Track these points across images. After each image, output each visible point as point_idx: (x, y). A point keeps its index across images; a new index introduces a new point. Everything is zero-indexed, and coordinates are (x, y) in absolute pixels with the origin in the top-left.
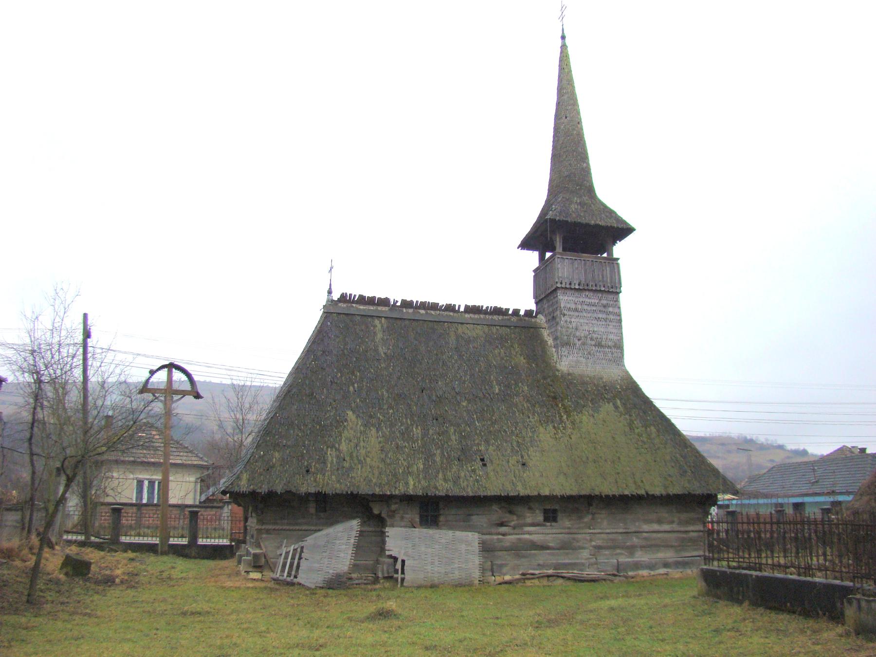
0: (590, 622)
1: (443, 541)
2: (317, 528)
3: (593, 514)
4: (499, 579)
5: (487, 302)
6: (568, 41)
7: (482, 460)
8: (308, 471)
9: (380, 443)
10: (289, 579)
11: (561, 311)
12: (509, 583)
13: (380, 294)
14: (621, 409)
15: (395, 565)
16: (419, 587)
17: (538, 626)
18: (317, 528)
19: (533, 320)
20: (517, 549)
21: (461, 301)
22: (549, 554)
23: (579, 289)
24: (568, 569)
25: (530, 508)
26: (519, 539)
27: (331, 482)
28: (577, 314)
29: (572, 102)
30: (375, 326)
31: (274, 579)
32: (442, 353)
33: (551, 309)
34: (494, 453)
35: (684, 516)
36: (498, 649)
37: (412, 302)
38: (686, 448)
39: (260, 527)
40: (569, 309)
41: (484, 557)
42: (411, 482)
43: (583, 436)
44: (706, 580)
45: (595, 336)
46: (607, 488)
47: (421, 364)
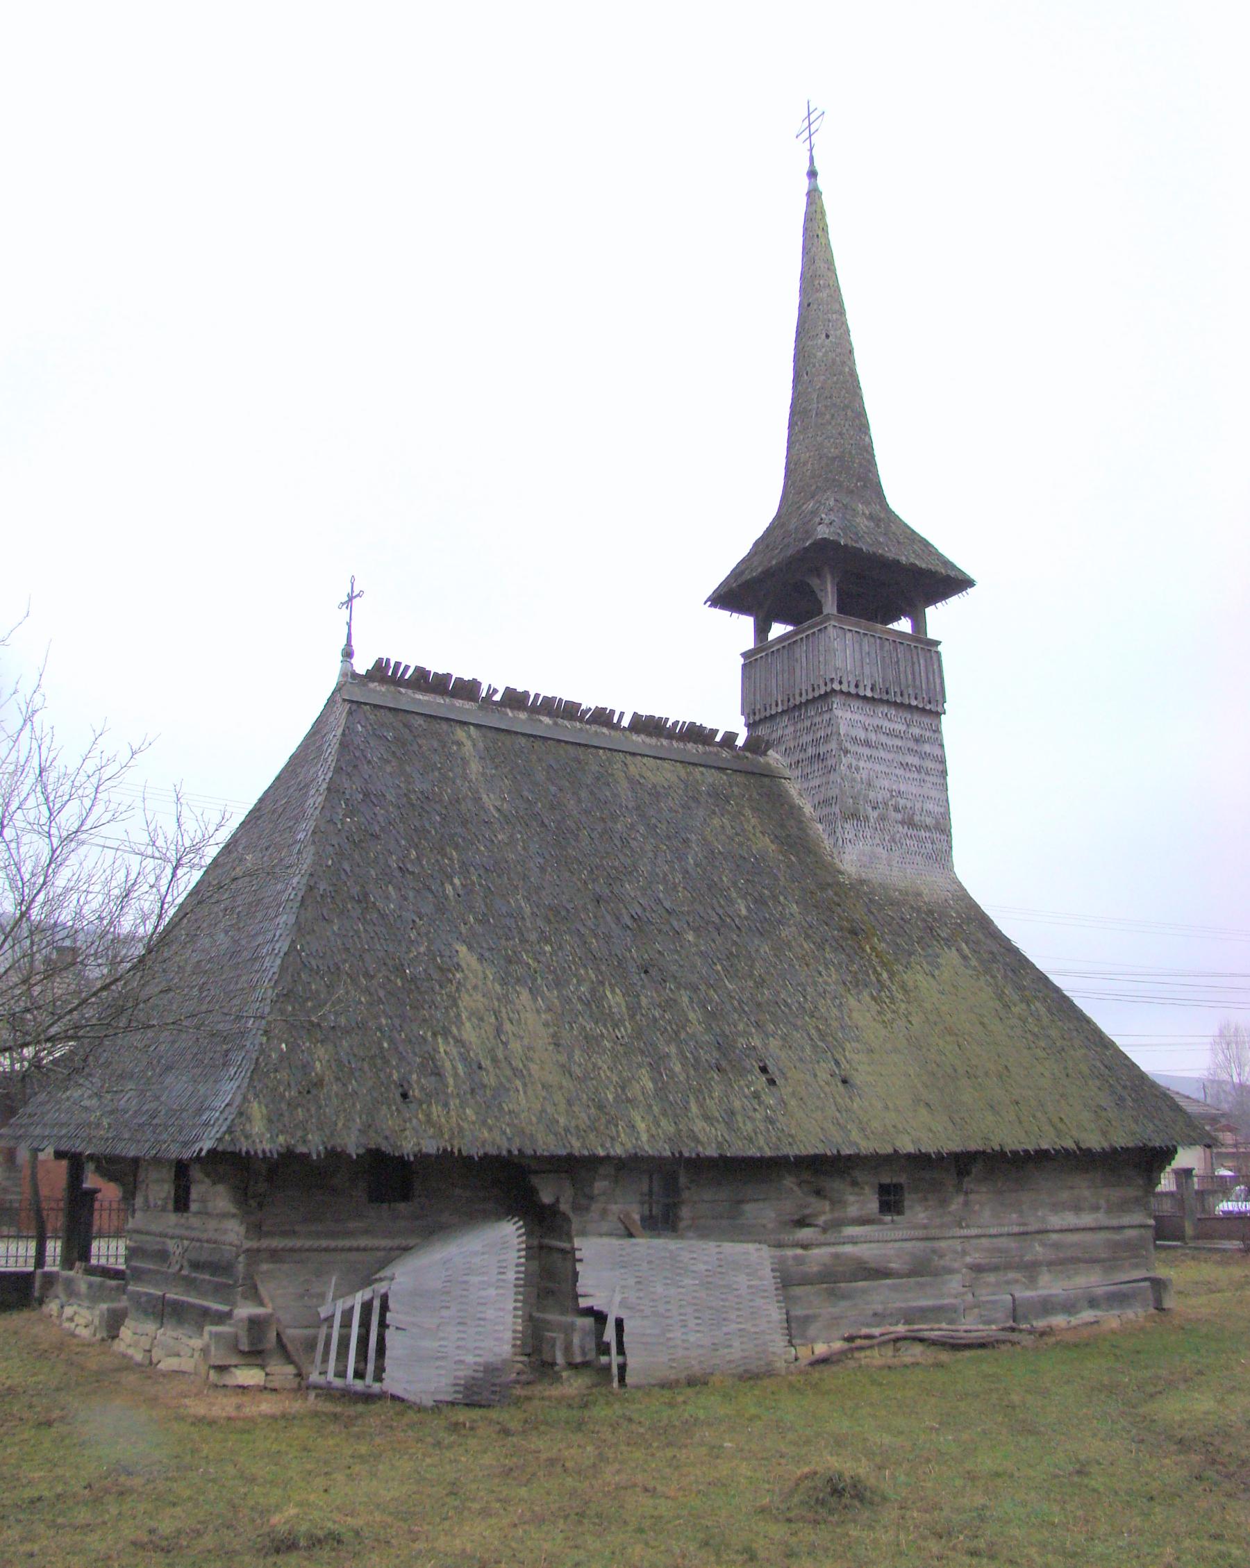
2: (404, 1242)
6: (821, 182)
7: (764, 1070)
8: (405, 1096)
9: (546, 1025)
10: (359, 1385)
11: (840, 743)
12: (824, 1361)
13: (461, 670)
23: (873, 699)
25: (854, 1183)
26: (836, 1256)
30: (459, 744)
32: (614, 818)
34: (783, 1055)
35: (1116, 1194)
39: (254, 1244)
40: (855, 740)
45: (902, 802)
46: (1013, 1138)
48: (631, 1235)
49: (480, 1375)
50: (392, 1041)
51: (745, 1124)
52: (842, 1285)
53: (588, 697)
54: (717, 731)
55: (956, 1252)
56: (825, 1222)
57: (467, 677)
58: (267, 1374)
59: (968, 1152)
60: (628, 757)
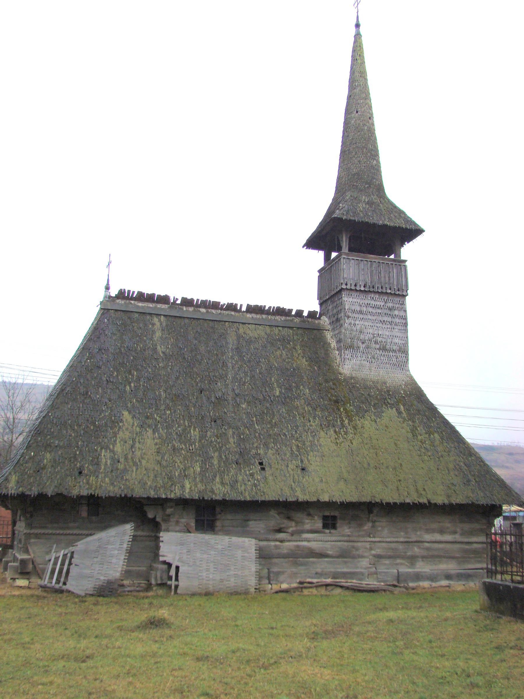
0: (369, 634)
1: (220, 547)
2: (90, 532)
3: (374, 522)
4: (276, 587)
5: (269, 301)
6: (362, 30)
7: (261, 464)
8: (80, 473)
9: (156, 444)
10: (57, 586)
11: (345, 314)
12: (286, 591)
14: (404, 415)
15: (169, 571)
16: (193, 595)
17: (314, 637)
18: (90, 532)
19: (316, 322)
20: (297, 556)
21: (243, 301)
22: (327, 562)
23: (365, 291)
24: (346, 578)
25: (309, 515)
26: (298, 546)
27: (105, 486)
28: (361, 316)
29: (363, 95)
30: (153, 325)
31: (42, 587)
33: (335, 311)
34: (273, 457)
35: (467, 526)
36: (272, 661)
37: (192, 300)
38: (471, 456)
39: (28, 531)
40: (354, 311)
41: (260, 564)
42: (188, 486)
43: (365, 441)
44: (488, 595)
45: (379, 339)
46: (389, 496)
47: (200, 364)
48: (190, 532)
49: (105, 584)
50: (81, 451)
51: (241, 486)
52: (301, 559)
53: (224, 299)
54: (292, 310)
55: (366, 548)
56: (292, 531)
57: (162, 294)
58: (30, 582)
59: (361, 502)
60: (241, 325)
